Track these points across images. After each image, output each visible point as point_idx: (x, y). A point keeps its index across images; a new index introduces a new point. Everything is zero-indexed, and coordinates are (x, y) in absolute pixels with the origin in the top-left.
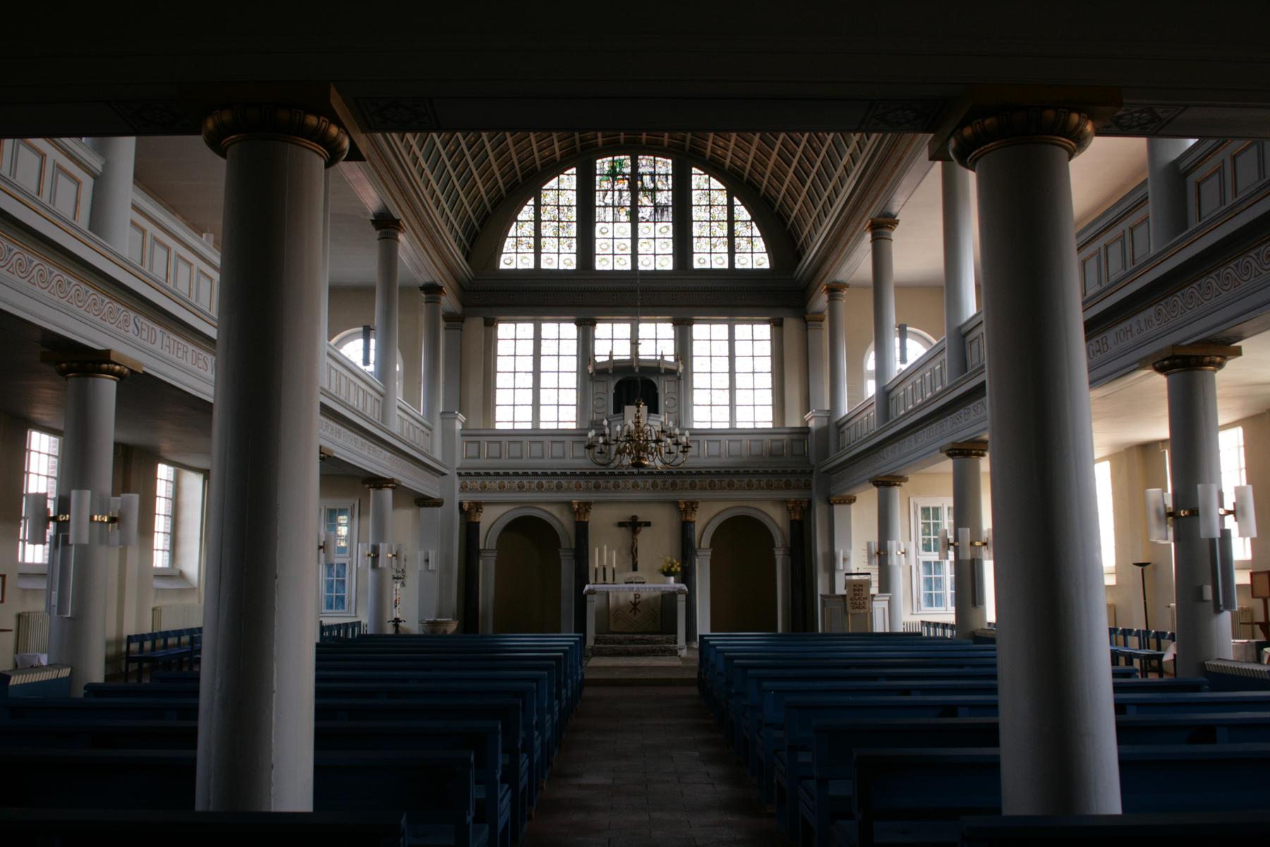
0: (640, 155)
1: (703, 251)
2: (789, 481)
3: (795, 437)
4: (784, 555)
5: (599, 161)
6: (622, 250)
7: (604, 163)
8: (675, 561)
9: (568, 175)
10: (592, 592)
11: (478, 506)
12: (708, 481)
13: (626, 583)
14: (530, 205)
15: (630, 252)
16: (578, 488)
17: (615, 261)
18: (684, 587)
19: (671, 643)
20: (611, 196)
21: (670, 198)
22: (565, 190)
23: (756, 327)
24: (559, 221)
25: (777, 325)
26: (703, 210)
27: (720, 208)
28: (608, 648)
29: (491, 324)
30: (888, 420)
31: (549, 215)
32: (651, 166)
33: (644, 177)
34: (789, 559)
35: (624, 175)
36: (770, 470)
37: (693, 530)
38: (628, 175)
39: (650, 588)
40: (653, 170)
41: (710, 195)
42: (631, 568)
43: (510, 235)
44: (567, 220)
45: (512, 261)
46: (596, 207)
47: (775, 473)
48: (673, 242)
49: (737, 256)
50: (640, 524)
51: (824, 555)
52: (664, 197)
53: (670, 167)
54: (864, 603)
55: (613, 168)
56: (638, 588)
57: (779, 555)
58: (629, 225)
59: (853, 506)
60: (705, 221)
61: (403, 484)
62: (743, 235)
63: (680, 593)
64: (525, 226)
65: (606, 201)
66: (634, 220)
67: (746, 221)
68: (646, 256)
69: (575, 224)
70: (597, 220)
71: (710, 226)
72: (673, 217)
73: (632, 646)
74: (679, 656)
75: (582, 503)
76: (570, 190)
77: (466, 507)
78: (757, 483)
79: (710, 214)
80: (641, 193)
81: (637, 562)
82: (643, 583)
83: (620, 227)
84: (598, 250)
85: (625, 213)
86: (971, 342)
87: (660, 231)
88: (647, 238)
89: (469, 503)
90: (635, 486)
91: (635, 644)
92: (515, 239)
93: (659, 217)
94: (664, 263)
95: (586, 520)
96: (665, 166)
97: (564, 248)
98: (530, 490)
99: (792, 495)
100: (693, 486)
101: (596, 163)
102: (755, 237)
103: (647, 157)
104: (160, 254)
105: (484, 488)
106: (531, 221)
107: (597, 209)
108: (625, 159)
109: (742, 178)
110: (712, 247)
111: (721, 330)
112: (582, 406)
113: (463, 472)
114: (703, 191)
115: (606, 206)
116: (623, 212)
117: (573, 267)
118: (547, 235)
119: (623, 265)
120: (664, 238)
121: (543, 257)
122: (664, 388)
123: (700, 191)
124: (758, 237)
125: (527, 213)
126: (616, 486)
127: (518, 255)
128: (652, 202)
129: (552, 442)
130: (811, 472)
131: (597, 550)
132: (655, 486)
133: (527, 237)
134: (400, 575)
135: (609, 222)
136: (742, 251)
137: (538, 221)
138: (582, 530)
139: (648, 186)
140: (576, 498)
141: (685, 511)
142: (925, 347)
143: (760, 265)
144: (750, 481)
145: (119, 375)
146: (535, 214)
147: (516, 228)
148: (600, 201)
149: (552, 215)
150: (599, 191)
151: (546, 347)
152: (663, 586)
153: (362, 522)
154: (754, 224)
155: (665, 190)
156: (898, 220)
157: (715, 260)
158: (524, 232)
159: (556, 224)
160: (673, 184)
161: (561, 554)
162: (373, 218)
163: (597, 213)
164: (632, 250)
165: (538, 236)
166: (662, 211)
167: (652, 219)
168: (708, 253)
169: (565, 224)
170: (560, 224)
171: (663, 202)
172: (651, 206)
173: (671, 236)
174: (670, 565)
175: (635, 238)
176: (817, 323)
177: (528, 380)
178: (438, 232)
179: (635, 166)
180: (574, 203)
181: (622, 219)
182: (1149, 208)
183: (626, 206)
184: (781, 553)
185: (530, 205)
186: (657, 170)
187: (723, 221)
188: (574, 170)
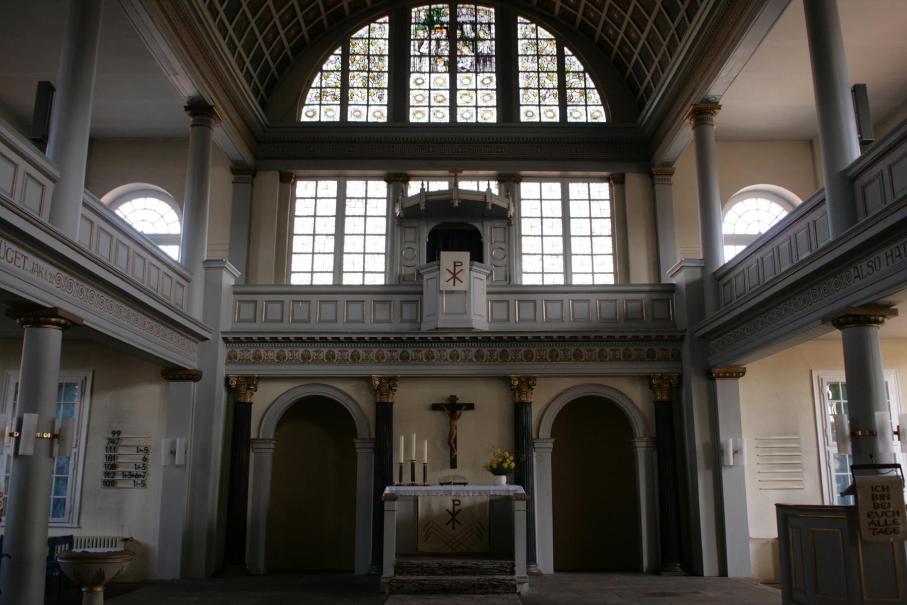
0: (460, 3)
1: (531, 104)
2: (652, 350)
3: (656, 296)
4: (647, 447)
5: (414, 10)
6: (440, 102)
7: (419, 11)
8: (507, 454)
9: (380, 23)
10: (393, 498)
11: (250, 382)
12: (548, 350)
13: (442, 484)
14: (337, 55)
15: (448, 104)
16: (380, 359)
17: (432, 113)
18: (520, 490)
19: (506, 573)
20: (427, 46)
21: (494, 48)
22: (376, 38)
23: (592, 185)
24: (369, 71)
25: (617, 182)
26: (530, 61)
27: (549, 58)
28: (413, 581)
29: (288, 181)
30: (719, 309)
31: (358, 65)
32: (472, 15)
33: (465, 26)
34: (655, 453)
35: (442, 23)
36: (629, 335)
37: (529, 414)
38: (447, 23)
39: (474, 492)
40: (474, 19)
41: (537, 45)
42: (449, 464)
43: (314, 85)
44: (378, 70)
45: (315, 113)
46: (411, 56)
47: (635, 339)
48: (497, 94)
49: (569, 109)
50: (460, 407)
51: (705, 446)
52: (486, 47)
53: (493, 16)
54: (894, 522)
55: (430, 16)
56: (458, 491)
57: (641, 448)
58: (447, 76)
59: (741, 380)
60: (532, 71)
61: (85, 323)
62: (576, 86)
63: (517, 499)
64: (330, 76)
65: (422, 50)
66: (453, 71)
67: (579, 72)
68: (466, 108)
69: (386, 75)
70: (411, 70)
71: (538, 77)
72: (496, 68)
73: (450, 578)
74: (519, 594)
75: (385, 378)
76: (382, 39)
77: (234, 384)
78: (612, 353)
79: (538, 64)
80: (461, 42)
81: (456, 456)
82: (465, 484)
83: (437, 78)
84: (412, 102)
85: (443, 63)
86: (724, 285)
87: (482, 82)
88: (468, 90)
89: (238, 378)
90: (454, 357)
91: (454, 574)
92: (319, 90)
93: (481, 67)
94: (487, 115)
95: (390, 400)
96: (487, 15)
97: (374, 100)
98: (317, 361)
99: (656, 368)
100: (528, 357)
101: (411, 12)
102: (590, 88)
103: (467, 6)
104: (104, 238)
105: (257, 359)
106: (338, 71)
107: (412, 59)
108: (443, 8)
109: (574, 23)
110: (541, 100)
111: (553, 189)
112: (391, 254)
113: (230, 337)
114: (530, 41)
115: (422, 55)
116: (441, 63)
117: (384, 120)
118: (355, 85)
119: (440, 118)
120: (487, 89)
121: (350, 109)
122: (490, 233)
123: (526, 41)
124: (592, 89)
125: (333, 63)
126: (429, 357)
127: (322, 107)
128: (473, 52)
129: (347, 301)
130: (682, 338)
131: (402, 439)
132: (479, 356)
133: (332, 88)
134: (140, 472)
135: (424, 73)
136: (574, 104)
137: (345, 71)
138: (384, 413)
139: (469, 35)
140: (377, 371)
141: (519, 389)
142: (785, 209)
143: (596, 118)
144: (602, 350)
145: (64, 327)
146: (342, 64)
147: (321, 78)
148: (415, 50)
149: (361, 65)
150: (414, 40)
151: (352, 207)
152: (492, 488)
153: (95, 399)
154: (587, 75)
155: (488, 39)
156: (721, 106)
157: (545, 113)
158: (330, 82)
159: (366, 74)
160: (496, 34)
161: (357, 445)
162: (187, 105)
163: (412, 63)
164: (450, 85)
165: (345, 87)
166: (485, 61)
167: (473, 69)
168: (536, 105)
169: (376, 74)
170: (370, 74)
171: (486, 52)
172: (472, 56)
173: (495, 87)
174: (501, 460)
175: (453, 89)
176: (665, 177)
177: (329, 244)
178: (201, 22)
179: (454, 15)
180: (386, 52)
181: (440, 69)
182: (827, 206)
183: (444, 56)
184: (644, 444)
185: (337, 55)
186: (478, 19)
187: (553, 72)
188: (387, 19)
